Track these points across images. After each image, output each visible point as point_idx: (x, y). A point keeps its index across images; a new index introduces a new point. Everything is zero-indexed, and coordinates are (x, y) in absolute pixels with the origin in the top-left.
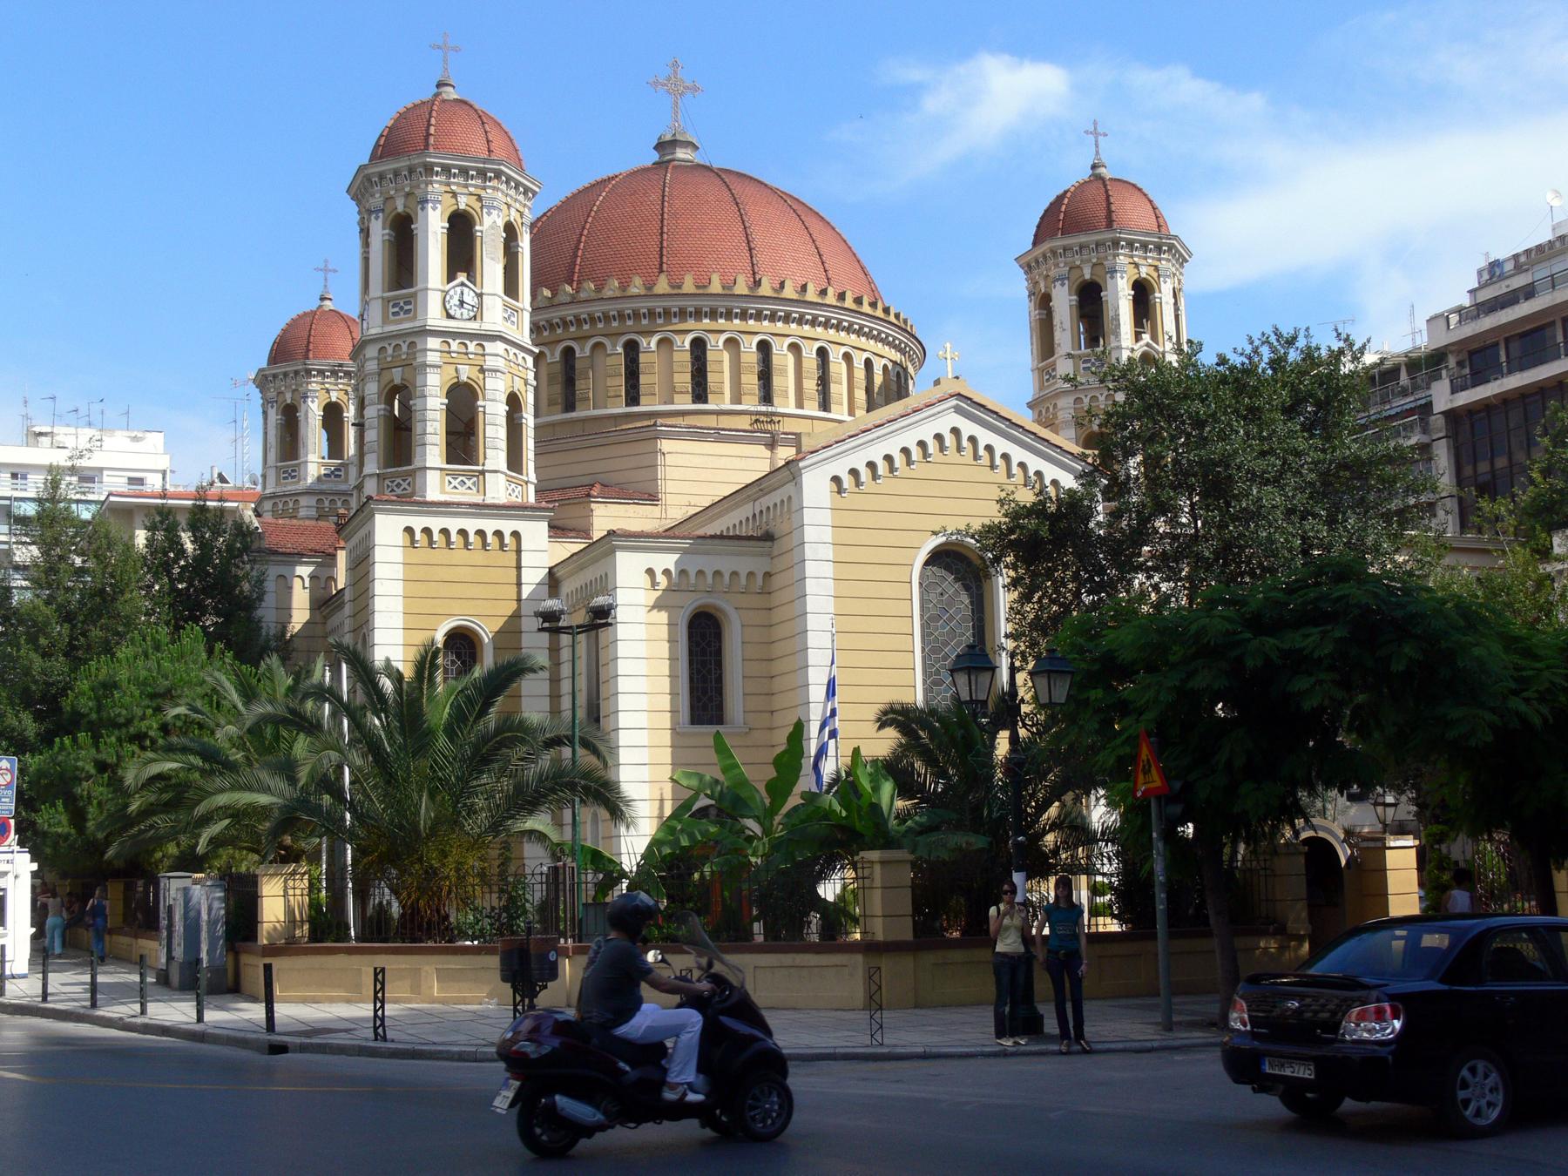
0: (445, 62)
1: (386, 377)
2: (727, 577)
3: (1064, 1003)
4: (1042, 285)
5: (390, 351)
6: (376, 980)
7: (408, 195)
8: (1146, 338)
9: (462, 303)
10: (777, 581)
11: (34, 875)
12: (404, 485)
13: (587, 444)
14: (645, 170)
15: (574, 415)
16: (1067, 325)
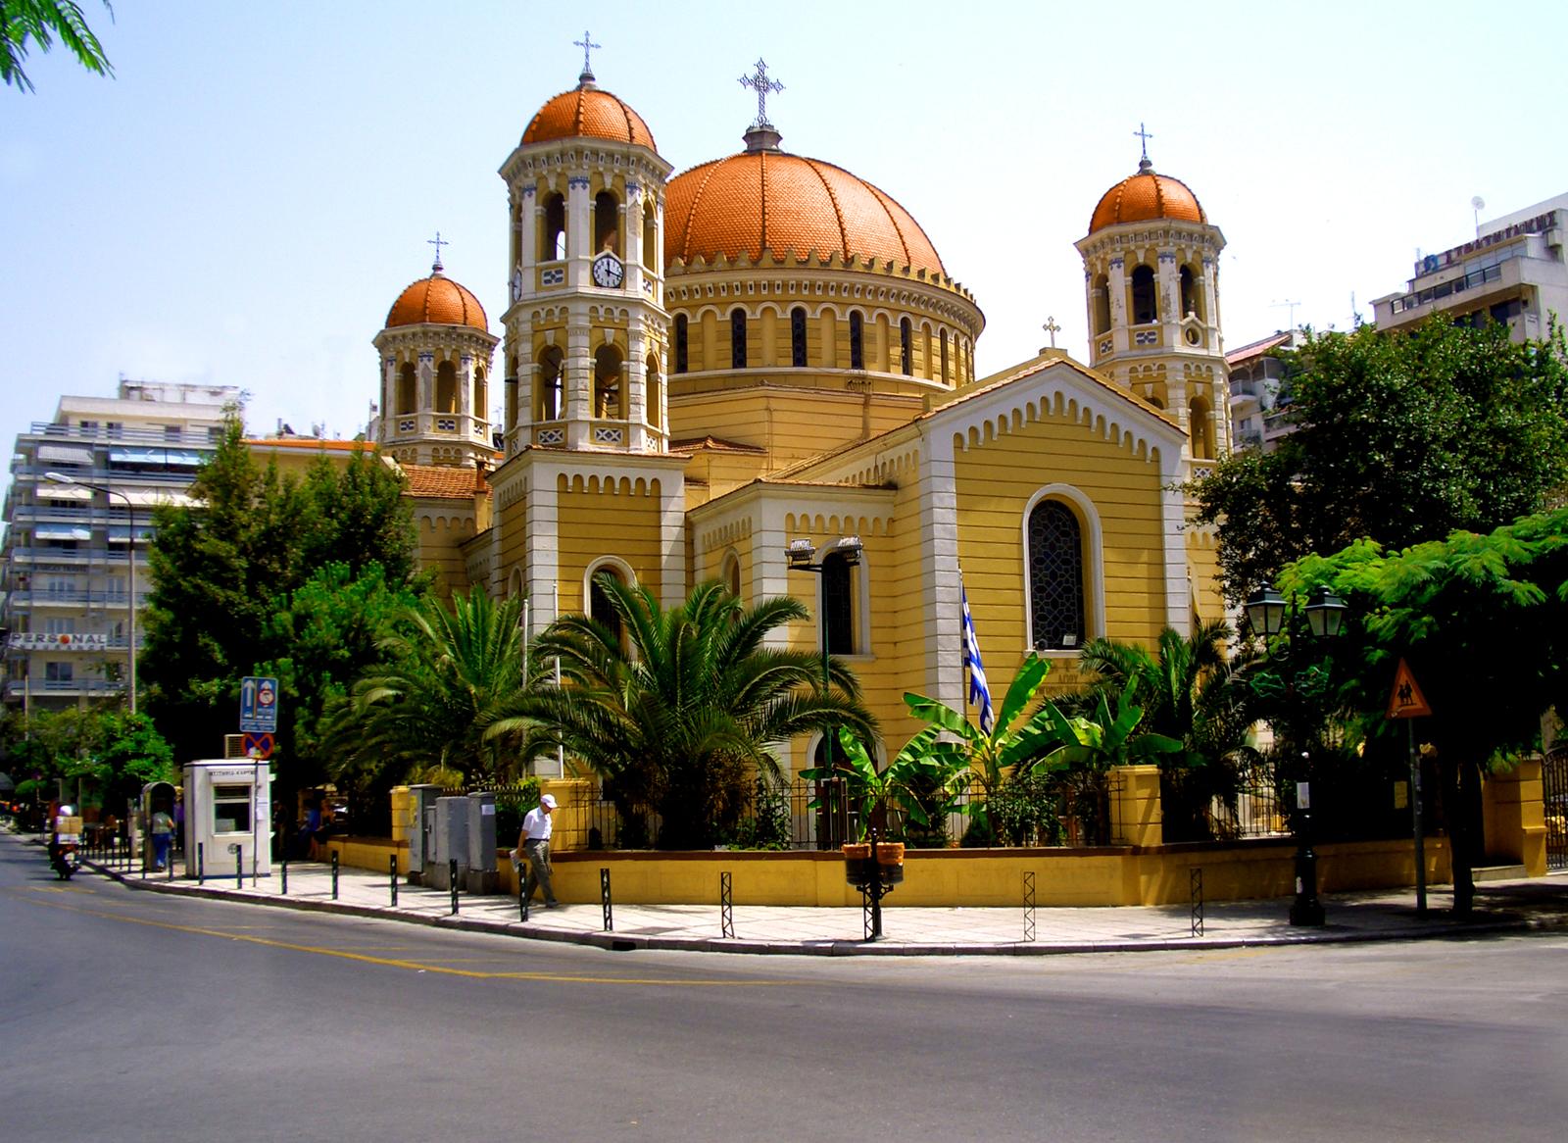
0: (587, 56)
1: (539, 337)
2: (857, 521)
3: (1505, 895)
4: (1099, 267)
5: (557, 312)
6: (608, 883)
7: (559, 175)
8: (1192, 314)
9: (609, 272)
10: (899, 527)
11: (273, 784)
12: (557, 436)
13: (838, 399)
14: (739, 156)
15: (686, 375)
16: (1123, 302)
